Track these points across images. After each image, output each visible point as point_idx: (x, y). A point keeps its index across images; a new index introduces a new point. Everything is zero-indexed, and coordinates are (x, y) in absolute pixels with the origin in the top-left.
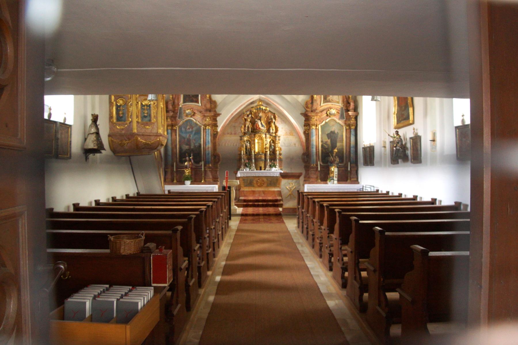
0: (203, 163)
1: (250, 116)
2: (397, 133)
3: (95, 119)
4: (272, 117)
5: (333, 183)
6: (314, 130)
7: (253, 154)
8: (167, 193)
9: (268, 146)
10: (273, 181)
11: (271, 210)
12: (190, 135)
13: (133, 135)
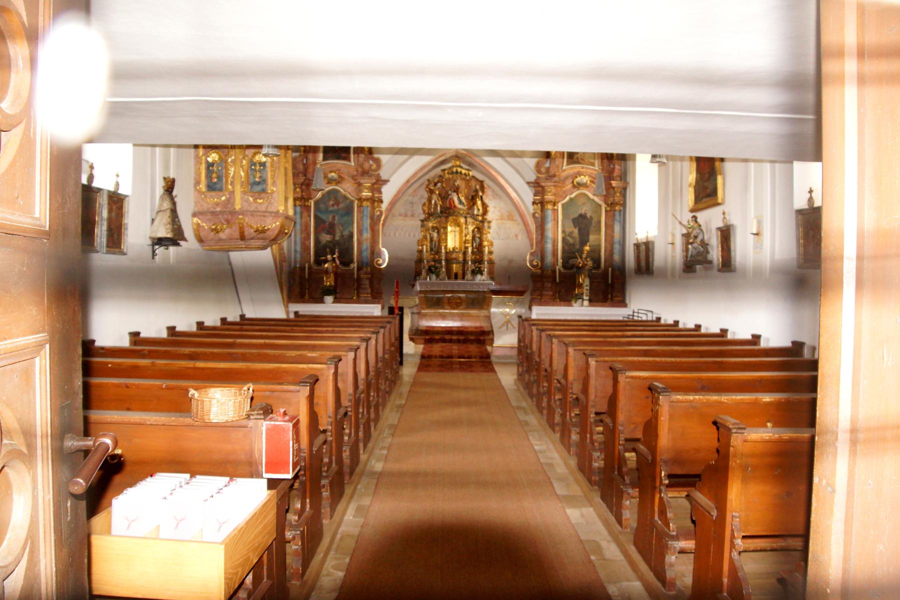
1: (439, 185)
2: (695, 218)
3: (170, 186)
4: (478, 187)
5: (582, 305)
7: (443, 251)
8: (292, 316)
9: (469, 237)
11: (473, 349)
12: (334, 218)
13: (234, 213)
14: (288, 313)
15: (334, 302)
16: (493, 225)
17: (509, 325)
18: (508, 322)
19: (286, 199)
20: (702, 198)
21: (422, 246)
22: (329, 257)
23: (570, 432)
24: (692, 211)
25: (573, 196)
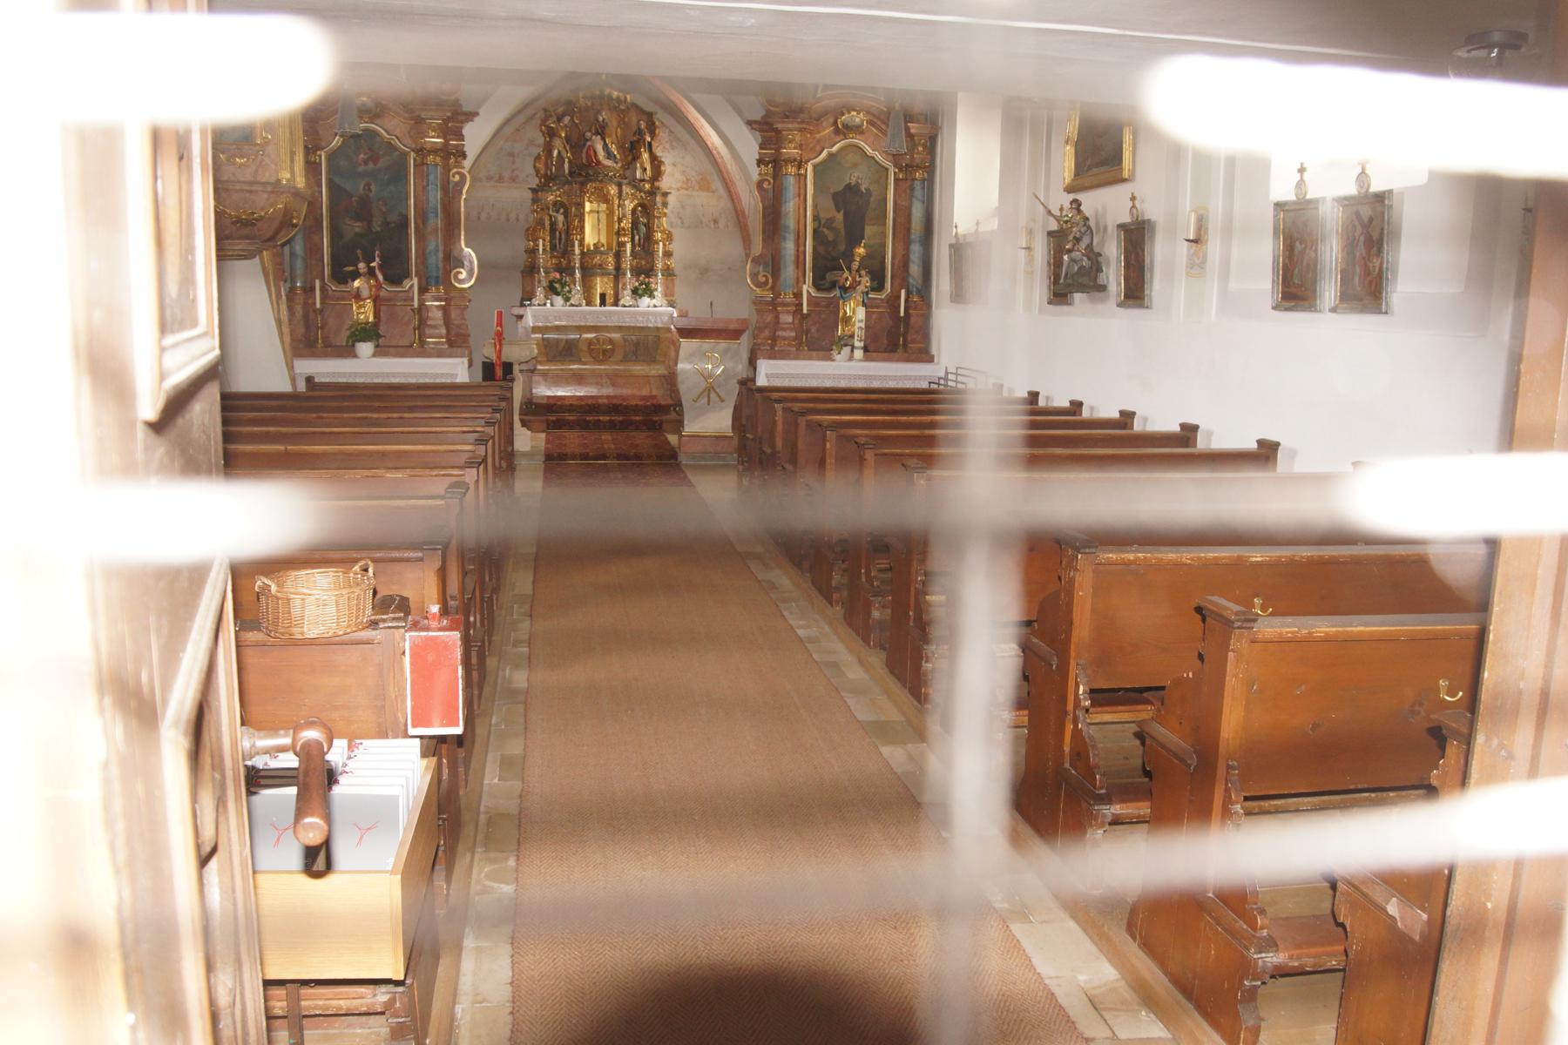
0: (415, 281)
1: (567, 119)
2: (1076, 204)
4: (643, 125)
5: (851, 358)
6: (791, 180)
7: (577, 251)
8: (302, 387)
9: (627, 224)
10: (647, 345)
11: (641, 439)
12: (368, 185)
14: (293, 380)
15: (374, 355)
16: (671, 199)
17: (713, 395)
18: (710, 389)
19: (293, 154)
20: (1090, 168)
21: (535, 240)
22: (362, 265)
23: (868, 607)
24: (1069, 190)
25: (834, 149)
